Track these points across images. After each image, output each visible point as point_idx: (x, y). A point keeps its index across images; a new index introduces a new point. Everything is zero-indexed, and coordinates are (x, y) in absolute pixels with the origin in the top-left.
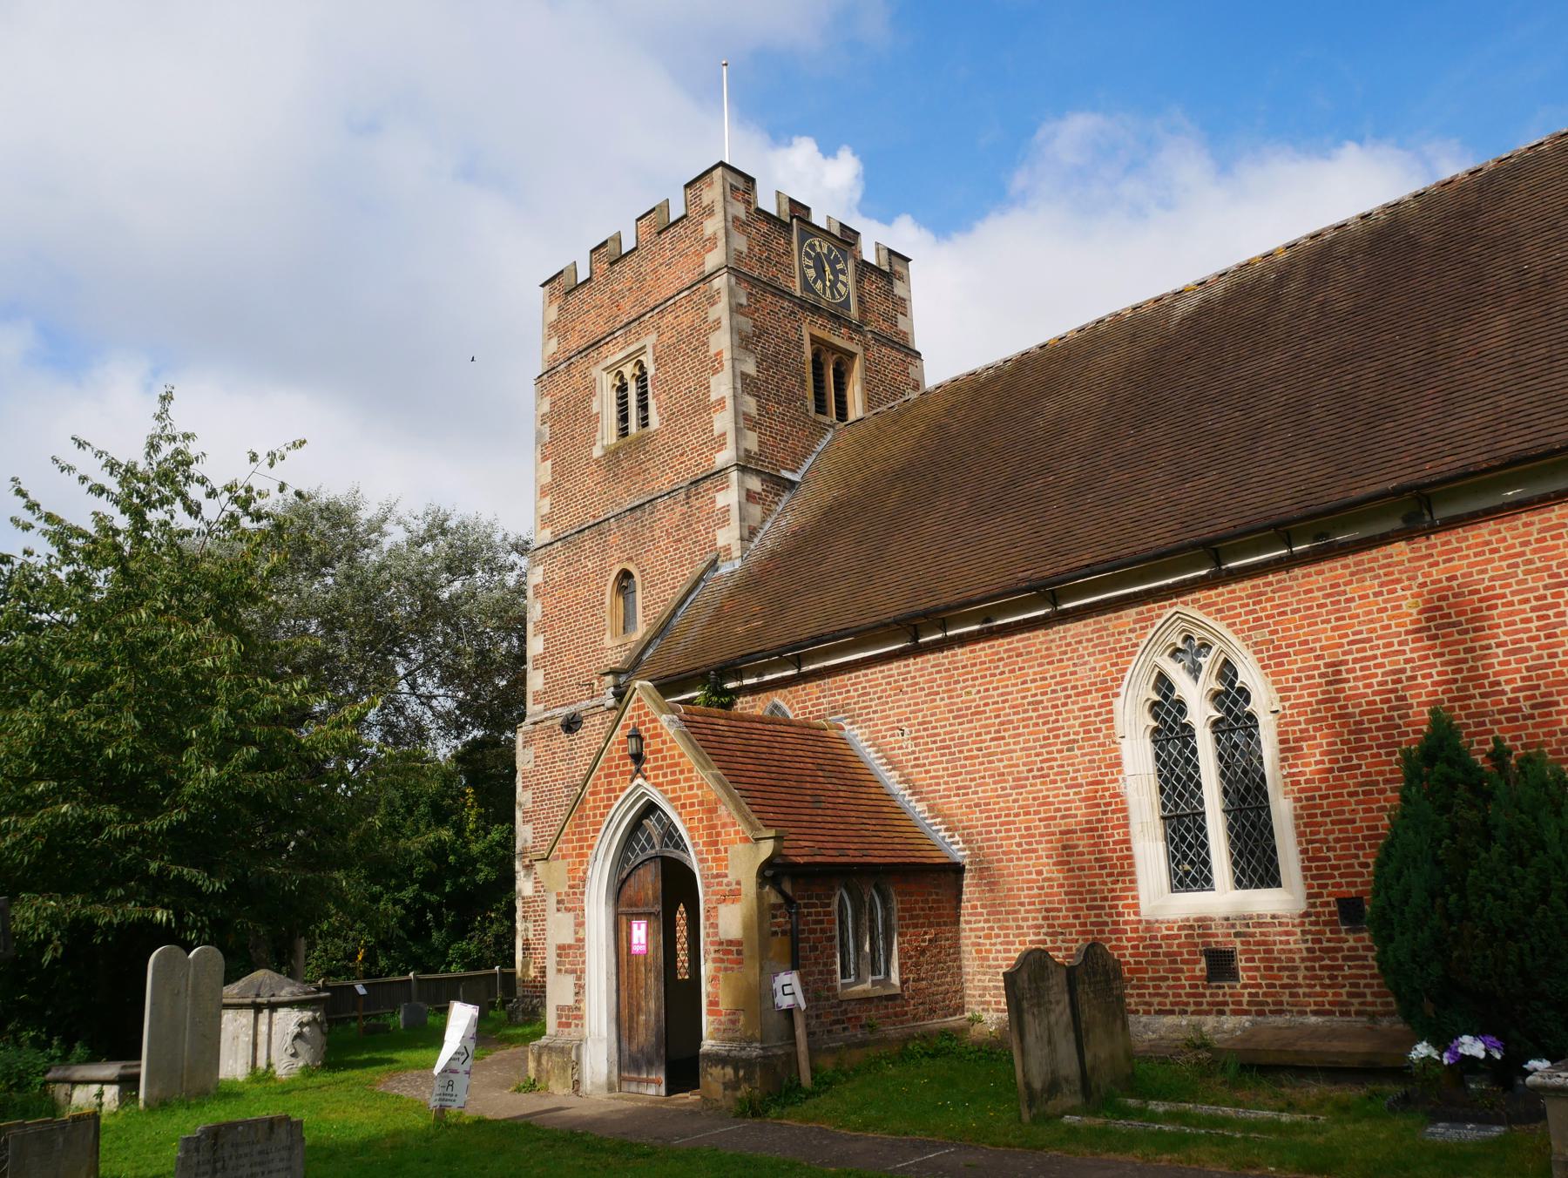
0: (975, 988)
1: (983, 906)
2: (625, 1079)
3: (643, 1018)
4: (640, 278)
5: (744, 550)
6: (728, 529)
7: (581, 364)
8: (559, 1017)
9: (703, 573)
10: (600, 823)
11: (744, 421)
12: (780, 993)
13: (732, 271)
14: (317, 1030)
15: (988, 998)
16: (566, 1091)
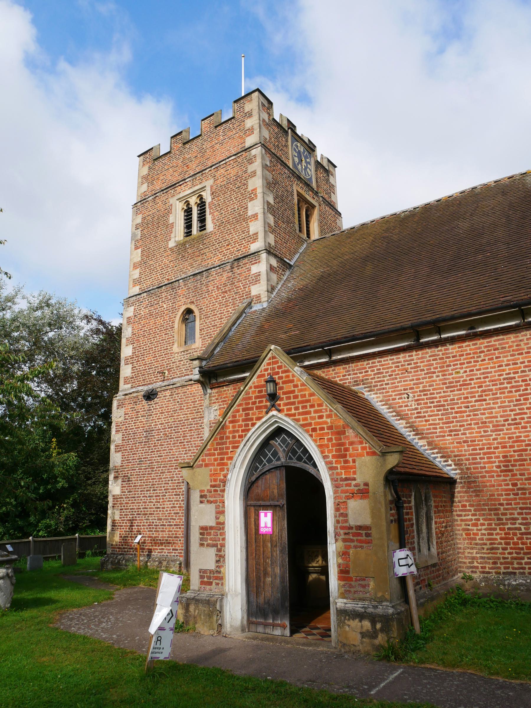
0: (466, 558)
1: (470, 505)
2: (253, 623)
3: (269, 579)
4: (202, 151)
5: (269, 297)
6: (260, 285)
7: (163, 197)
8: (202, 577)
9: (245, 309)
10: (239, 442)
11: (269, 229)
12: (397, 565)
13: (263, 146)
14: (8, 582)
15: (476, 564)
16: (211, 632)
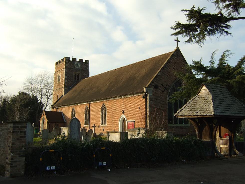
11: (65, 83)
